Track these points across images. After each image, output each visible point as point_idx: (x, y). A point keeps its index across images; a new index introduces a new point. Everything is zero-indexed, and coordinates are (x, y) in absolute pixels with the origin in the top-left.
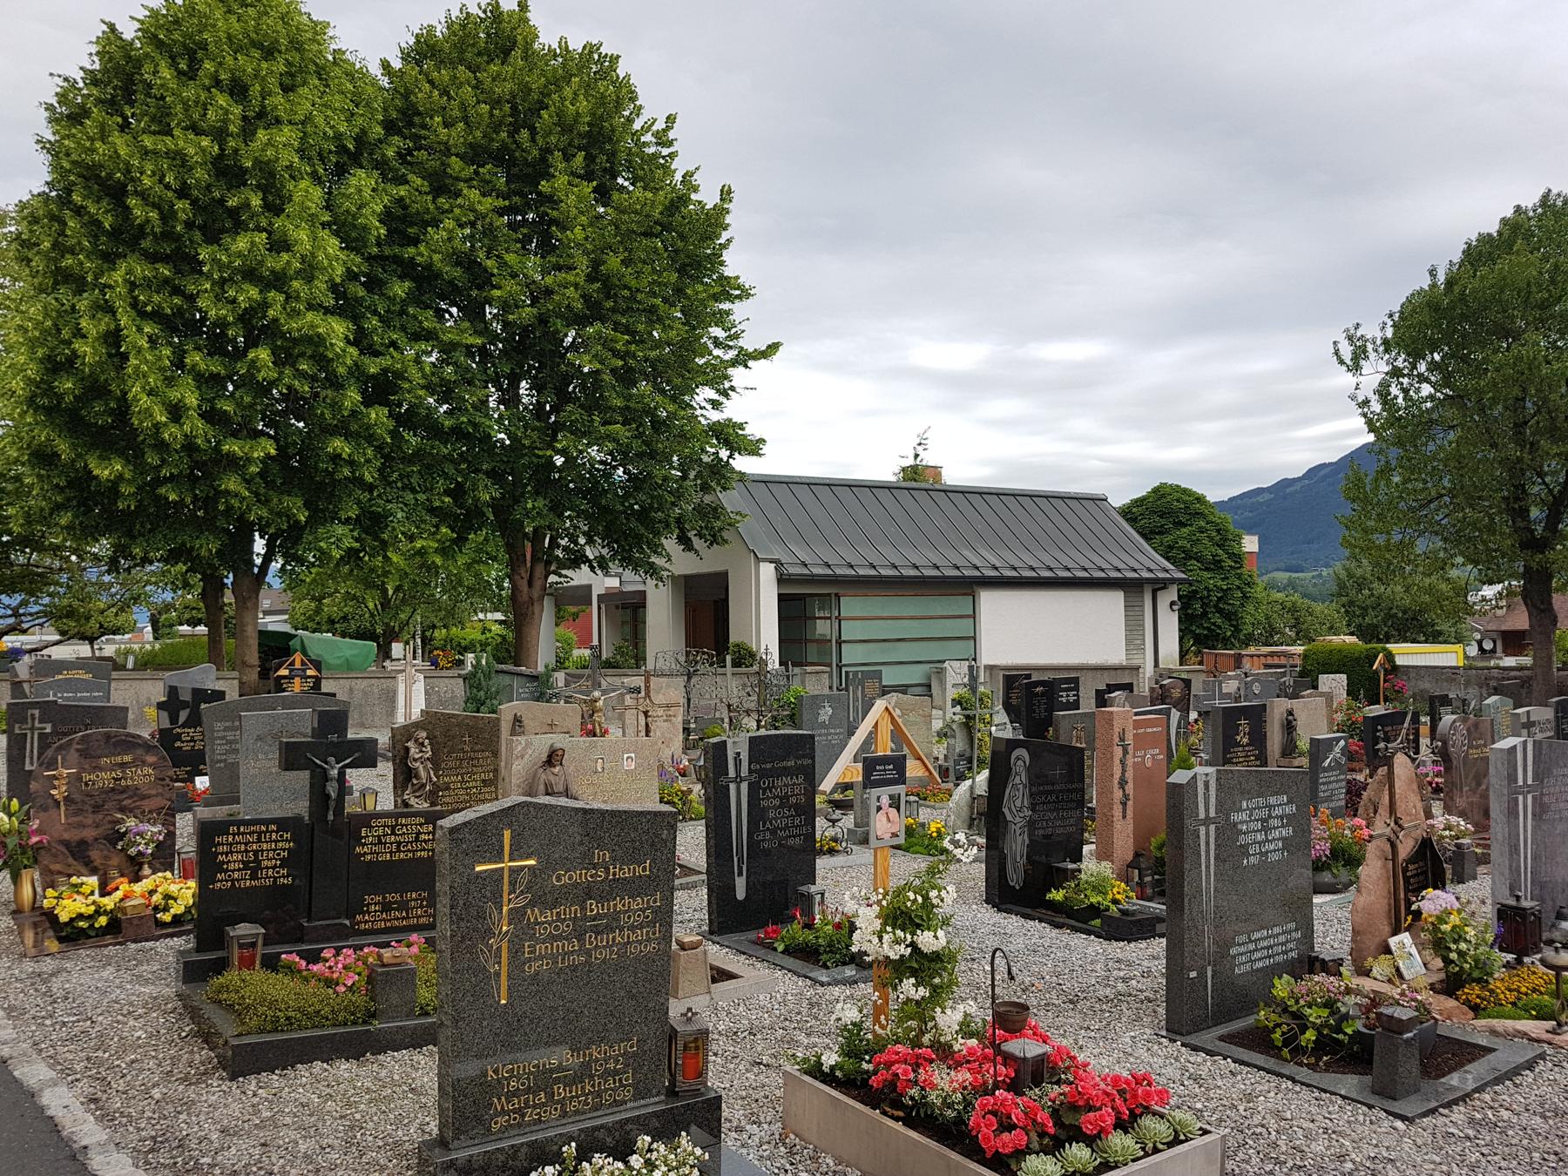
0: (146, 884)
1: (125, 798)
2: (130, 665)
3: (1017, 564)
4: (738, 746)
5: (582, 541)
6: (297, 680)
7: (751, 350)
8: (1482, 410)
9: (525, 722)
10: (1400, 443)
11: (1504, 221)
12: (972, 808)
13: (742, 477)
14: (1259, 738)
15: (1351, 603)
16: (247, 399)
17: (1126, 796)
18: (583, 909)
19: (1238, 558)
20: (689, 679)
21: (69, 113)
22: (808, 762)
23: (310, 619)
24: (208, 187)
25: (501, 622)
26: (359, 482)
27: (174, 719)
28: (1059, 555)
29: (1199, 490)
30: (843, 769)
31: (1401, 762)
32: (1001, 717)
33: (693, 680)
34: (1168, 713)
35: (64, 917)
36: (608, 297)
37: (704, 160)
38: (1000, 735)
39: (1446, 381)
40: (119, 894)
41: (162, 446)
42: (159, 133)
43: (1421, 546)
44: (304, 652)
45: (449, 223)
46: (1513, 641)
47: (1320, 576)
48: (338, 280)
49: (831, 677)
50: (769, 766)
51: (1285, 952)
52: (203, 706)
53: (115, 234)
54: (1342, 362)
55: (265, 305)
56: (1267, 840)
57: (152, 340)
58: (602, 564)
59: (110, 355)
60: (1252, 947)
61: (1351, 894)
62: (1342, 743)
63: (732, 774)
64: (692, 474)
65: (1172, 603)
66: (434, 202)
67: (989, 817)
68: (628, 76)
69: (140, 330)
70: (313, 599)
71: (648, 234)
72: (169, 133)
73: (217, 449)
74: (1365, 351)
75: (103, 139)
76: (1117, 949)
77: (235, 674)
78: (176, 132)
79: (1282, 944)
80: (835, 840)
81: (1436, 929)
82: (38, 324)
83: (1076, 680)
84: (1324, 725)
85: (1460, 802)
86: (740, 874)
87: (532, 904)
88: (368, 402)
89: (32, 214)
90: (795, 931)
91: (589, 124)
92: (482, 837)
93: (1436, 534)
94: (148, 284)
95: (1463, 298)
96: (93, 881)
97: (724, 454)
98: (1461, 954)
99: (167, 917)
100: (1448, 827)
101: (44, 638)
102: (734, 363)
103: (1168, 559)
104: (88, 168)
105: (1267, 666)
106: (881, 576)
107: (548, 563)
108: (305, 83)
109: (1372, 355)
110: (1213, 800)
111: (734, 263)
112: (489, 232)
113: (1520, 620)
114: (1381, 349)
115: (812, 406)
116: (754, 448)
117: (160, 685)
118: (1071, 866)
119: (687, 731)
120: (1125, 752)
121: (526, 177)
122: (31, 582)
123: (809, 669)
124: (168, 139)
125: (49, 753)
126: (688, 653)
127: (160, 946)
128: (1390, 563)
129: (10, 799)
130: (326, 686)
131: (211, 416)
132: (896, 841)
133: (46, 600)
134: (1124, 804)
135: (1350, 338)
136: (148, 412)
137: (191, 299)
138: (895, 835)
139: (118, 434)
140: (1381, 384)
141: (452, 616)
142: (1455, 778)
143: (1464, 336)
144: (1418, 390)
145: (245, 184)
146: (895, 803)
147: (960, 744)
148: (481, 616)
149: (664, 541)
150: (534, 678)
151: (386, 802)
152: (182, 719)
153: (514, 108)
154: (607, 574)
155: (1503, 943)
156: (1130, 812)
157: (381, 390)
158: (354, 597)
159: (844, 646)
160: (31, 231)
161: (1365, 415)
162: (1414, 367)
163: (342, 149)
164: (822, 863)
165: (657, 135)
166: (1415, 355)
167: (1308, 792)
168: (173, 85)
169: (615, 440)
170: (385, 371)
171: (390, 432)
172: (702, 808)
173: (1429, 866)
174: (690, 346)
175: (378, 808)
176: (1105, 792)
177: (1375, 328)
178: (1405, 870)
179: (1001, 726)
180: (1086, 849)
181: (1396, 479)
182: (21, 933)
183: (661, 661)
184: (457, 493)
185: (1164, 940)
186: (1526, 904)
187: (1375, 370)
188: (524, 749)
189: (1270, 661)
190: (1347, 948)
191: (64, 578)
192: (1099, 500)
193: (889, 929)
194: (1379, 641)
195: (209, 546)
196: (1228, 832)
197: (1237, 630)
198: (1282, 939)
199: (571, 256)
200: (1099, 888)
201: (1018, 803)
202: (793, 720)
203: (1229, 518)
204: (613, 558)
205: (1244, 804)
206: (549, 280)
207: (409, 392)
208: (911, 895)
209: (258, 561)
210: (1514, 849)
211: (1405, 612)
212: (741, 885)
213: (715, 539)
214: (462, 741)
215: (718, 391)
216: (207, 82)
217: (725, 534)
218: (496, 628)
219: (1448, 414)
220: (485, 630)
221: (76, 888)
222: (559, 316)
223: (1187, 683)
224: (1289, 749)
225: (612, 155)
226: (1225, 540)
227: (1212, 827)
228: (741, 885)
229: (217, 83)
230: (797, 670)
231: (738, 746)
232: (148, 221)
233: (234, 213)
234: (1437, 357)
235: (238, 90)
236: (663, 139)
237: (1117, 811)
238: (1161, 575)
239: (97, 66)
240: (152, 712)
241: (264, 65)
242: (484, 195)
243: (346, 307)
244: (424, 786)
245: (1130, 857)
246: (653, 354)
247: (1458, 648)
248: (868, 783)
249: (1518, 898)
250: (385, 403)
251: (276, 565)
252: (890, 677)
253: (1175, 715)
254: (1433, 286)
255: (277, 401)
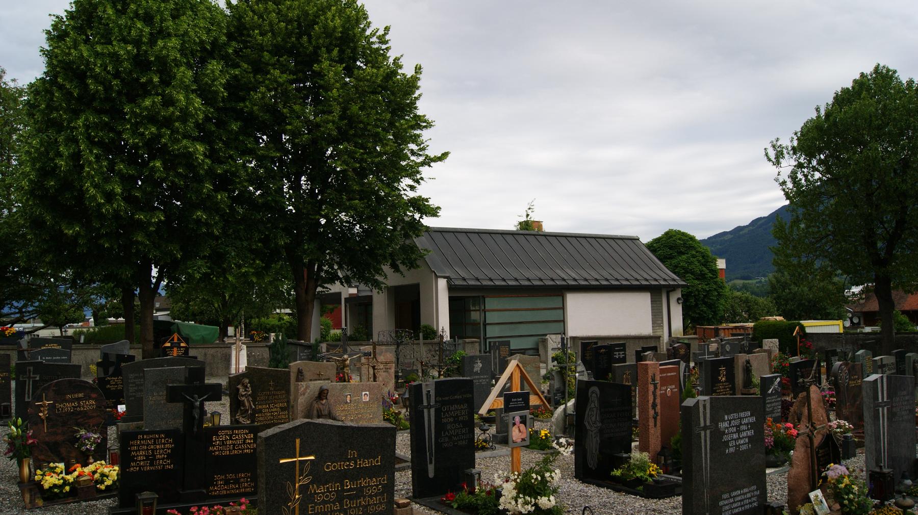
0: (91, 467)
1: (81, 418)
2: (82, 341)
3: (588, 277)
4: (428, 387)
5: (336, 267)
6: (175, 349)
7: (432, 156)
8: (848, 187)
9: (305, 373)
10: (804, 205)
11: (855, 81)
12: (565, 421)
13: (428, 229)
14: (731, 377)
15: (779, 297)
16: (149, 189)
17: (656, 413)
18: (342, 485)
19: (715, 272)
20: (398, 347)
21: (58, 34)
22: (469, 396)
23: (183, 313)
24: (131, 72)
25: (289, 314)
26: (211, 235)
27: (106, 372)
28: (612, 271)
29: (691, 233)
30: (492, 401)
31: (813, 389)
32: (581, 368)
33: (401, 347)
34: (678, 363)
35: (46, 486)
36: (351, 128)
37: (405, 52)
38: (581, 378)
39: (828, 170)
40: (76, 474)
41: (101, 217)
42: (105, 43)
43: (817, 264)
44: (179, 333)
45: (263, 89)
46: (869, 318)
47: (760, 282)
48: (200, 121)
49: (480, 345)
50: (447, 398)
51: (750, 503)
52: (123, 364)
53: (80, 99)
54: (769, 160)
55: (160, 136)
56: (740, 438)
57: (97, 157)
58: (347, 281)
59: (75, 166)
60: (731, 500)
61: (786, 467)
62: (778, 379)
63: (425, 403)
64: (399, 228)
65: (678, 299)
66: (254, 77)
67: (574, 426)
68: (363, 6)
69: (91, 152)
70: (184, 302)
71: (374, 92)
72: (110, 43)
73: (132, 217)
74: (782, 154)
75: (75, 48)
76: (652, 504)
77: (140, 346)
78: (114, 43)
79: (749, 498)
80: (485, 441)
81: (835, 487)
82: (37, 150)
83: (624, 345)
84: (767, 369)
85: (845, 412)
86: (431, 463)
87: (312, 482)
88: (217, 189)
89: (36, 90)
90: (464, 496)
91: (341, 32)
92: (284, 443)
93: (826, 257)
94: (96, 126)
95: (835, 124)
96: (61, 466)
97: (417, 216)
98: (850, 501)
99: (103, 487)
100: (839, 426)
101: (36, 325)
102: (423, 164)
103: (675, 273)
104: (67, 63)
105: (733, 335)
106: (509, 286)
107: (317, 280)
108: (184, 14)
109: (786, 156)
110: (708, 415)
111: (423, 108)
112: (285, 93)
113: (874, 306)
114: (791, 152)
115: (474, 178)
116: (434, 212)
117: (98, 353)
118: (625, 455)
119: (397, 377)
120: (655, 388)
121: (306, 62)
122: (29, 294)
123: (467, 340)
124: (110, 47)
125: (39, 392)
126: (397, 332)
127: (99, 503)
128: (800, 274)
129: (17, 419)
130: (192, 353)
131: (129, 199)
132: (525, 444)
133: (37, 304)
134: (655, 418)
135: (774, 146)
136: (94, 198)
137: (119, 133)
138: (523, 440)
139: (78, 210)
140: (792, 172)
141: (263, 311)
142: (845, 399)
143: (837, 144)
144: (813, 176)
145: (150, 70)
146: (524, 421)
147: (557, 384)
148: (278, 311)
149: (383, 267)
150: (309, 347)
151: (226, 421)
152: (110, 373)
153: (299, 26)
154: (350, 286)
155: (872, 494)
156: (659, 424)
157: (224, 182)
158: (207, 301)
159: (488, 327)
160: (36, 99)
161: (784, 190)
162: (810, 162)
163: (204, 49)
164: (478, 455)
165: (379, 38)
166: (810, 155)
167: (759, 409)
168: (113, 18)
169: (355, 209)
170: (226, 171)
171: (228, 206)
172: (408, 423)
173: (832, 450)
174: (399, 155)
175: (221, 424)
176: (644, 411)
177: (788, 141)
178: (817, 453)
179: (580, 373)
180: (633, 444)
181: (802, 226)
182: (23, 495)
183: (382, 336)
184: (266, 241)
185: (680, 498)
186: (886, 470)
187: (789, 164)
188: (305, 390)
189: (734, 332)
190: (785, 499)
191: (47, 291)
192: (634, 240)
193: (521, 496)
194: (796, 319)
195: (127, 273)
196: (717, 435)
197: (715, 313)
198: (749, 495)
199: (330, 106)
200: (642, 467)
201: (593, 419)
202: (459, 371)
203: (709, 249)
204: (354, 277)
205: (726, 417)
206: (318, 119)
207: (239, 183)
208: (534, 476)
209: (154, 281)
210: (878, 439)
211: (809, 302)
212: (431, 469)
213: (412, 265)
214: (268, 383)
215: (413, 180)
216: (131, 15)
217: (418, 262)
218: (286, 317)
219: (830, 189)
220: (280, 319)
221: (53, 470)
222: (324, 139)
223: (688, 346)
224: (748, 382)
225: (354, 50)
226: (707, 262)
227: (708, 432)
228: (431, 469)
229: (137, 15)
230: (460, 341)
231: (428, 387)
232: (97, 91)
233: (144, 85)
234: (822, 157)
235: (148, 19)
236: (382, 40)
237: (651, 423)
238: (672, 283)
239: (74, 9)
240: (93, 368)
241: (163, 5)
242: (282, 73)
243: (206, 138)
244: (247, 411)
245: (659, 449)
246: (377, 160)
247: (840, 322)
248: (508, 409)
249: (881, 467)
250: (226, 190)
251: (164, 283)
252: (515, 344)
253: (683, 365)
254: (819, 117)
255: (166, 190)
